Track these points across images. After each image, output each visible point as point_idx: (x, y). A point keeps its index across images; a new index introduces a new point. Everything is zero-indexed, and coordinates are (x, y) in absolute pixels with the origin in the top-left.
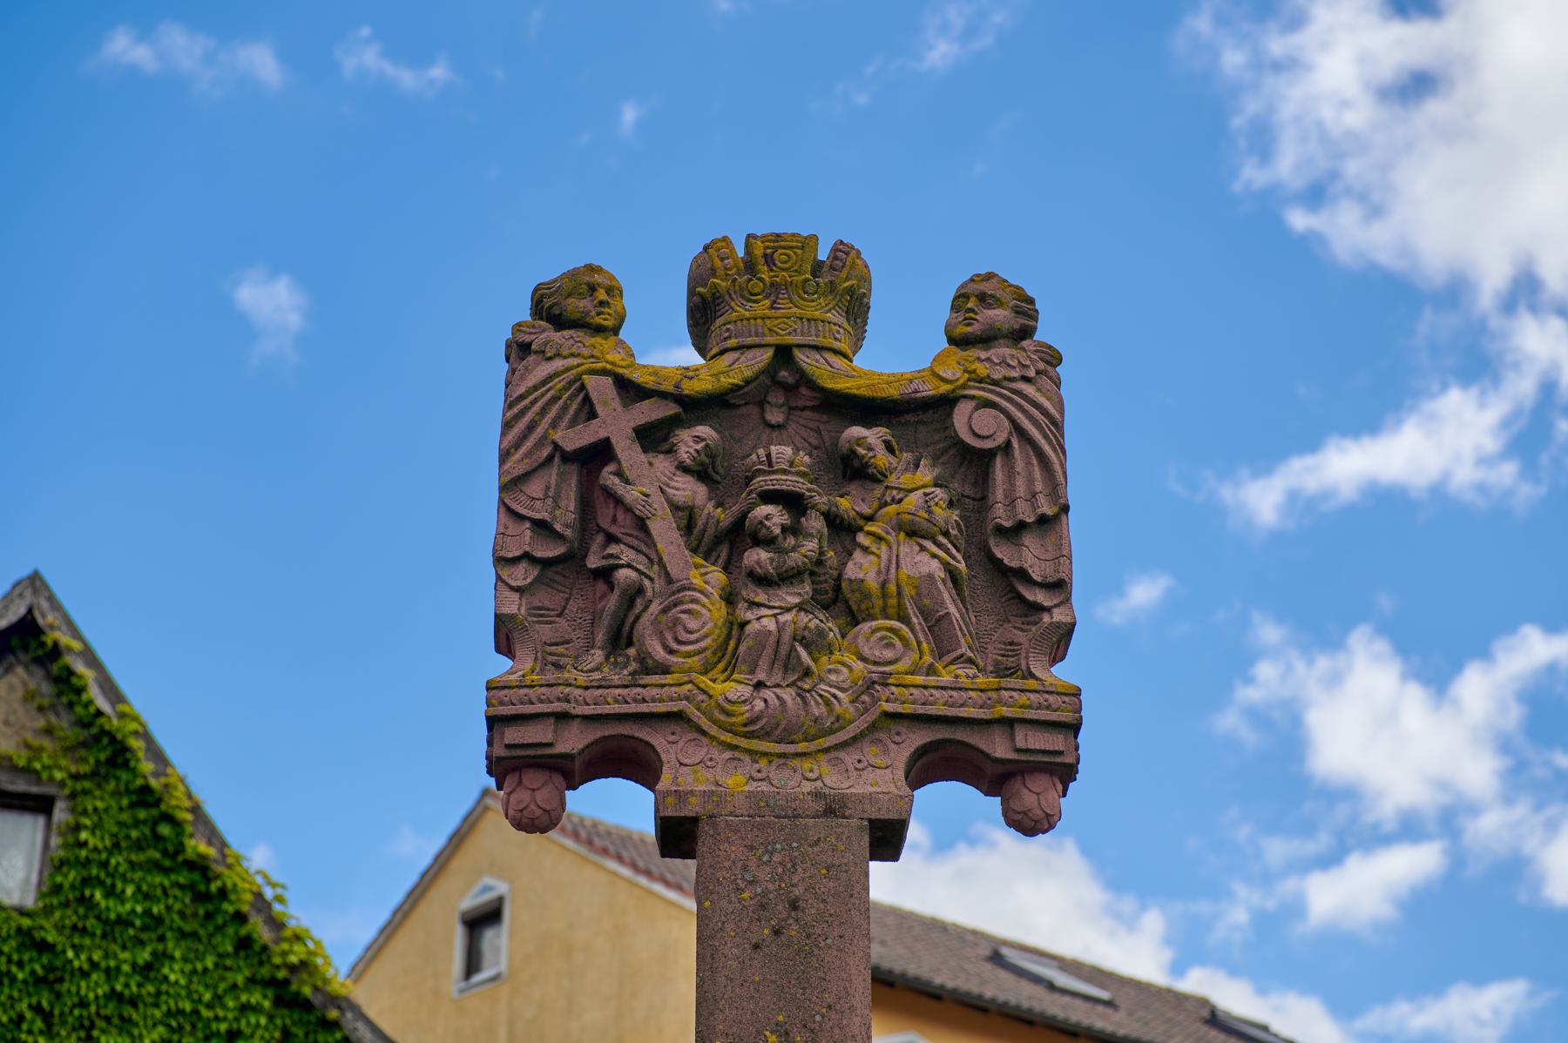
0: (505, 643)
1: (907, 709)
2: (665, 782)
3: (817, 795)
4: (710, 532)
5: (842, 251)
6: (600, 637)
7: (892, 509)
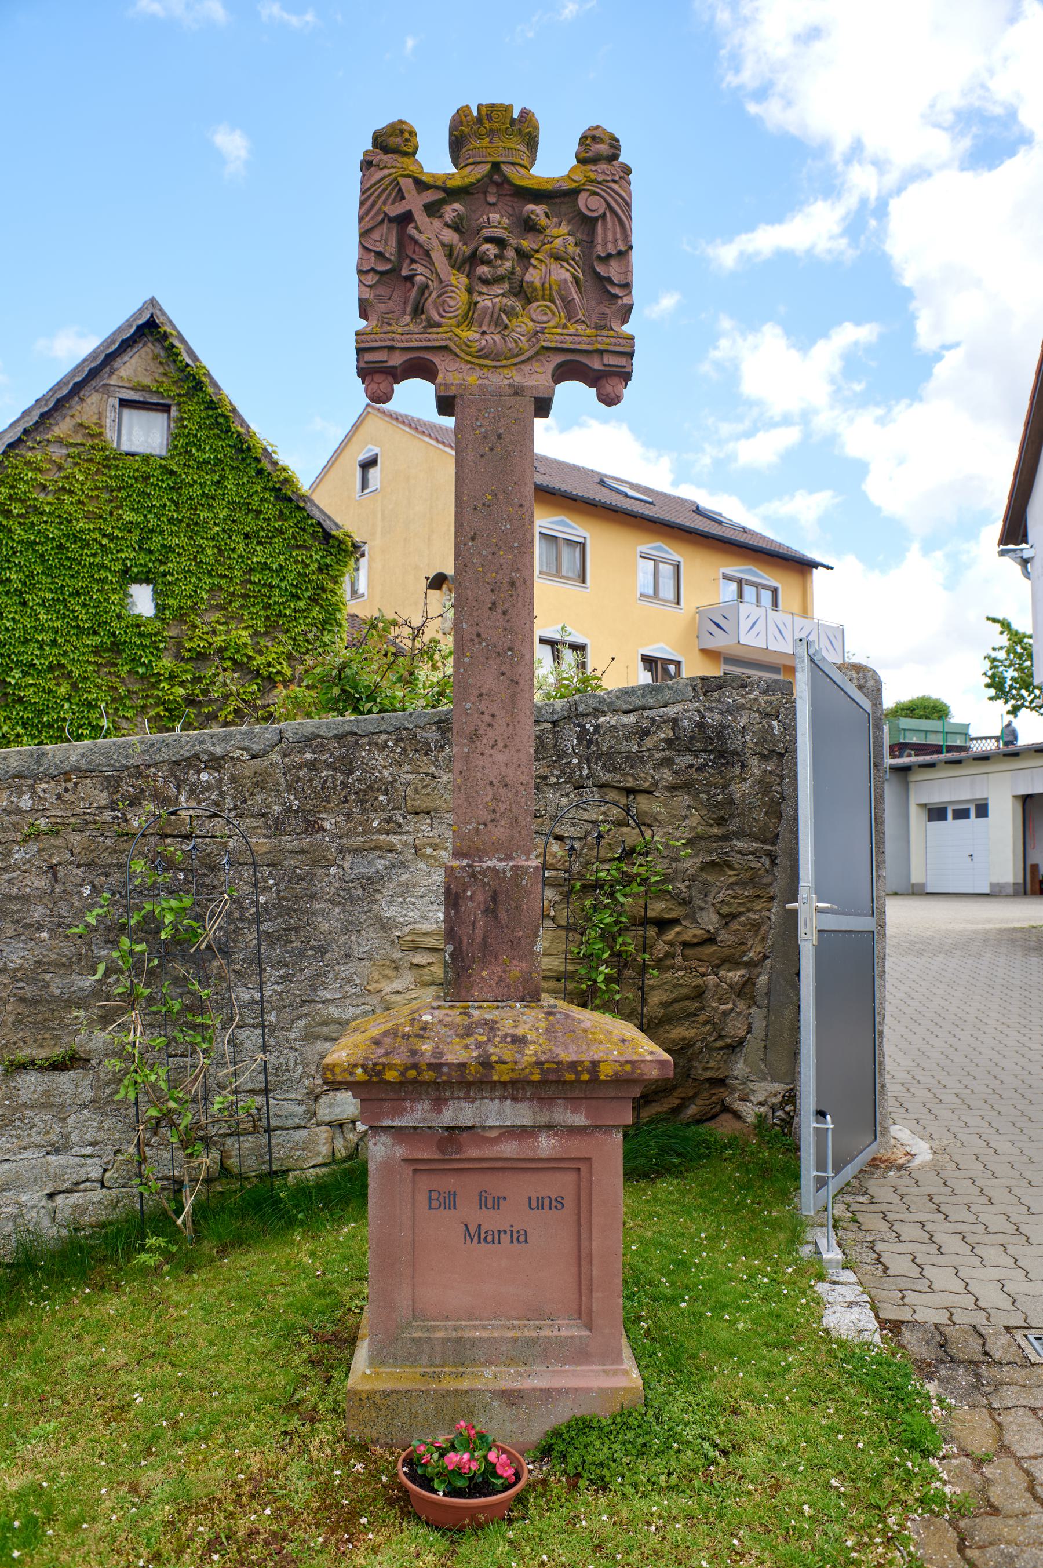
0: (364, 314)
1: (553, 345)
2: (440, 379)
3: (510, 386)
4: (459, 260)
5: (525, 113)
6: (409, 309)
7: (548, 246)
